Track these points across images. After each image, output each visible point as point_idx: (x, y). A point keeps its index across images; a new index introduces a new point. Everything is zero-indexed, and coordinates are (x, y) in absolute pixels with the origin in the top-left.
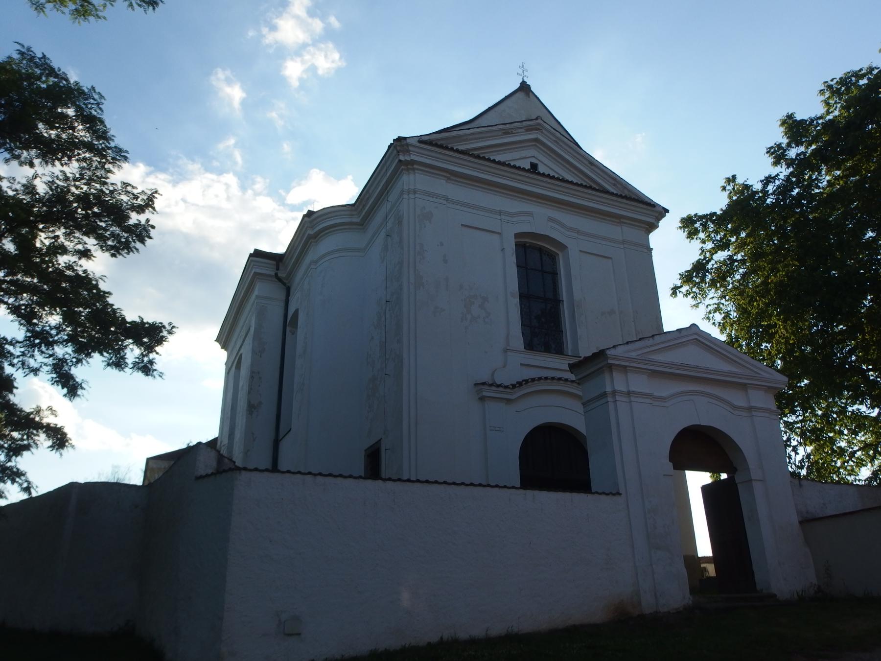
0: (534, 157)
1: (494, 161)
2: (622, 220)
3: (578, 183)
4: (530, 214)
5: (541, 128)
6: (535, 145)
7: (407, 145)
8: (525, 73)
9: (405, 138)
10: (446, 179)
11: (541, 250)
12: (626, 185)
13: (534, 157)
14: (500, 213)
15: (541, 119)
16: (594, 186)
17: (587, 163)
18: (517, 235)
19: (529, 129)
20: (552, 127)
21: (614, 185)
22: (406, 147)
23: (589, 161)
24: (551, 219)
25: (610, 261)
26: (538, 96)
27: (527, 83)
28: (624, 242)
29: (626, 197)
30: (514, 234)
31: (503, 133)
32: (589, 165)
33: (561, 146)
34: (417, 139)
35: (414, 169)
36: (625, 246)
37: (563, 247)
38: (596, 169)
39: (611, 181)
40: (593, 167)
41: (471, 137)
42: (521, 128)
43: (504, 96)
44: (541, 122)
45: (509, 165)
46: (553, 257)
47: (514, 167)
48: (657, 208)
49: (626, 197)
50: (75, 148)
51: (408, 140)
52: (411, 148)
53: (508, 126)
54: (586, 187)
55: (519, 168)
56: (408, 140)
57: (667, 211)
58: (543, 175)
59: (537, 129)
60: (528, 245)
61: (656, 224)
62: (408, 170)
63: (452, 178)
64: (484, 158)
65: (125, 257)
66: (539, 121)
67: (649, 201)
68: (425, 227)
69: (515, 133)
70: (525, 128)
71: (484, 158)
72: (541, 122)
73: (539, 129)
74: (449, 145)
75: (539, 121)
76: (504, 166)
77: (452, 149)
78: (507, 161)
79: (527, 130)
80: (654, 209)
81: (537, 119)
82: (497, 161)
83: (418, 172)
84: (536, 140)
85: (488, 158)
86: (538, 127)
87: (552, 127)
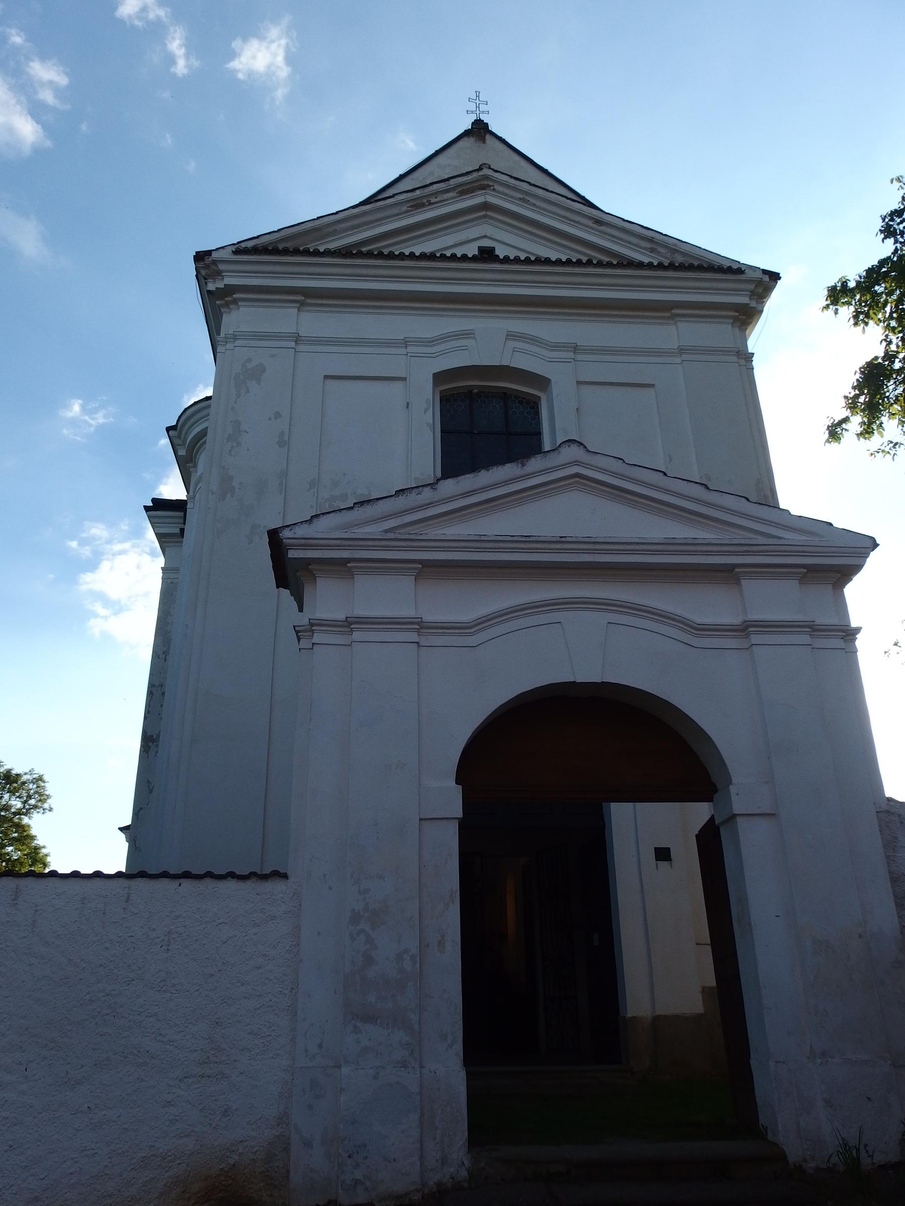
0: (485, 236)
1: (412, 256)
2: (675, 311)
3: (703, 266)
4: (470, 334)
5: (491, 184)
6: (485, 216)
7: (215, 262)
8: (483, 108)
9: (209, 253)
10: (298, 305)
11: (505, 396)
12: (675, 245)
13: (485, 236)
14: (406, 343)
15: (490, 168)
16: (606, 259)
17: (590, 223)
18: (439, 378)
19: (466, 190)
20: (511, 177)
21: (652, 250)
22: (213, 267)
23: (594, 218)
24: (511, 336)
25: (651, 391)
26: (503, 137)
27: (485, 122)
28: (681, 351)
29: (682, 267)
30: (868, 326)
31: (412, 206)
32: (595, 226)
33: (534, 205)
34: (230, 249)
35: (235, 301)
36: (685, 357)
37: (543, 382)
38: (609, 230)
39: (644, 244)
40: (602, 228)
41: (343, 226)
42: (447, 191)
43: (434, 151)
44: (490, 172)
45: (443, 257)
46: (533, 405)
47: (453, 257)
48: (749, 274)
49: (682, 267)
50: (884, 309)
51: (215, 255)
52: (222, 267)
53: (418, 192)
54: (579, 263)
55: (464, 258)
56: (215, 255)
57: (775, 277)
58: (506, 260)
59: (484, 187)
60: (475, 391)
61: (759, 308)
62: (227, 305)
63: (309, 301)
64: (391, 256)
65: (425, 412)
66: (486, 171)
67: (727, 264)
68: (248, 391)
69: (436, 203)
70: (457, 191)
71: (391, 256)
72: (490, 172)
73: (489, 186)
74: (384, 251)
75: (486, 171)
76: (403, 259)
77: (316, 253)
78: (438, 251)
79: (462, 193)
80: (742, 277)
81: (480, 169)
82: (470, 256)
83: (244, 303)
84: (486, 206)
85: (451, 255)
86: (486, 183)
87: (511, 177)
